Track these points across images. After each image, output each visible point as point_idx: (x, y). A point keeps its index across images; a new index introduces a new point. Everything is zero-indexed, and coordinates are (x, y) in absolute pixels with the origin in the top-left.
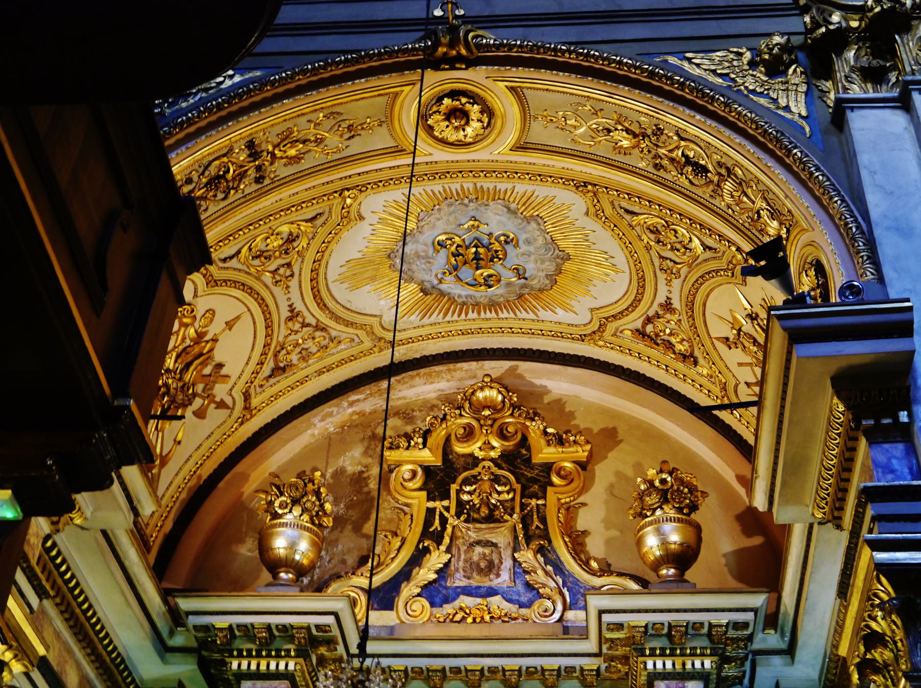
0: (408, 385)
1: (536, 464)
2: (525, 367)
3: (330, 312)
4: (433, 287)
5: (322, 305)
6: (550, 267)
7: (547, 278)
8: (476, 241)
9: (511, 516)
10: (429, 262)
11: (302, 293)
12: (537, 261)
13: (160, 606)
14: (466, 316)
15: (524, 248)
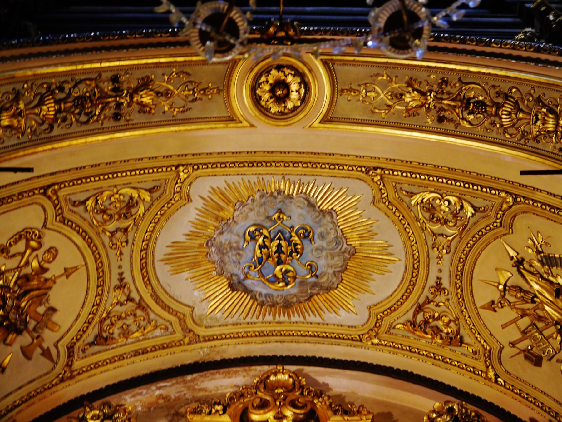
0: (210, 378)
2: (308, 370)
3: (152, 289)
4: (240, 282)
5: (148, 282)
6: (338, 263)
7: (335, 275)
8: (280, 234)
10: (239, 254)
11: (131, 264)
12: (328, 256)
14: (263, 319)
15: (318, 242)
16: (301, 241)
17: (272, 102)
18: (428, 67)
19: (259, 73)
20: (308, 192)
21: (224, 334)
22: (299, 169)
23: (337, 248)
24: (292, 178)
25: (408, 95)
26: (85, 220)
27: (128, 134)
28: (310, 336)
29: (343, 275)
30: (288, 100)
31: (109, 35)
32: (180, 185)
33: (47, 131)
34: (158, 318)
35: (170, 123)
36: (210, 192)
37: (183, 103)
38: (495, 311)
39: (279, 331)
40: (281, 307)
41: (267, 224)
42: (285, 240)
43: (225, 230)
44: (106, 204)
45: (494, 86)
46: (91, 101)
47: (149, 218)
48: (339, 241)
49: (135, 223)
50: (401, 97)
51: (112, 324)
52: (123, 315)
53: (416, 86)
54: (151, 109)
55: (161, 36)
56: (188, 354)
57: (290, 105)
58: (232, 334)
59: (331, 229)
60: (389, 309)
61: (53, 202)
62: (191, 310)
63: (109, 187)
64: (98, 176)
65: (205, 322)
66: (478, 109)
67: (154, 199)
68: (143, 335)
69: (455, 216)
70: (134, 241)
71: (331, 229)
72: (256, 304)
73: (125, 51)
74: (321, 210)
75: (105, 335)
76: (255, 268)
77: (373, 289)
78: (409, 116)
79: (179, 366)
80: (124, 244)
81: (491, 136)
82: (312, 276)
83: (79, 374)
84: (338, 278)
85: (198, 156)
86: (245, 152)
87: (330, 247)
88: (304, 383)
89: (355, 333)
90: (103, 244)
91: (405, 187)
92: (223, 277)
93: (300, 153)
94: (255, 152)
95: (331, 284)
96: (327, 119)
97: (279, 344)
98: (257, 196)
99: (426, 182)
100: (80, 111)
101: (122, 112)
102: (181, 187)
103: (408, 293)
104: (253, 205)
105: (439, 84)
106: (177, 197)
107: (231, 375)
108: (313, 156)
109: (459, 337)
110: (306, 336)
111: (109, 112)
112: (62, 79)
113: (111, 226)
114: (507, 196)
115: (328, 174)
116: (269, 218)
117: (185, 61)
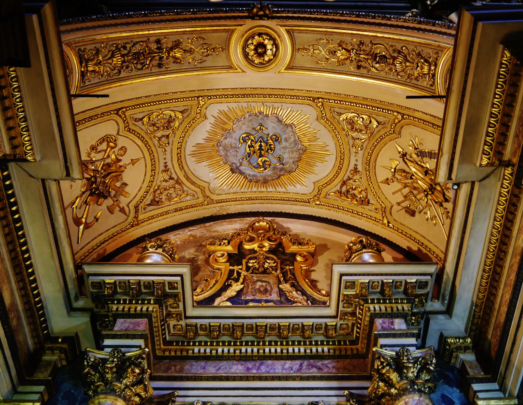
1: (287, 253)
2: (278, 219)
4: (237, 168)
5: (182, 168)
9: (276, 272)
10: (236, 151)
12: (289, 152)
13: (72, 272)
15: (284, 144)
16: (274, 143)
18: (352, 34)
24: (268, 104)
25: (339, 52)
28: (279, 200)
37: (201, 57)
39: (261, 197)
41: (253, 132)
42: (264, 142)
44: (155, 120)
45: (392, 46)
46: (144, 55)
51: (161, 193)
52: (168, 188)
53: (344, 46)
55: (186, 14)
56: (207, 210)
57: (267, 59)
61: (123, 119)
62: (208, 184)
64: (150, 103)
65: (216, 192)
66: (382, 60)
67: (184, 117)
69: (366, 127)
72: (247, 181)
74: (286, 124)
75: (157, 199)
77: (316, 172)
80: (167, 145)
83: (142, 222)
84: (295, 165)
87: (291, 147)
89: (305, 198)
90: (154, 144)
91: (337, 110)
96: (289, 67)
98: (247, 116)
105: (358, 44)
110: (277, 200)
111: (155, 63)
112: (125, 41)
113: (159, 134)
117: (202, 30)
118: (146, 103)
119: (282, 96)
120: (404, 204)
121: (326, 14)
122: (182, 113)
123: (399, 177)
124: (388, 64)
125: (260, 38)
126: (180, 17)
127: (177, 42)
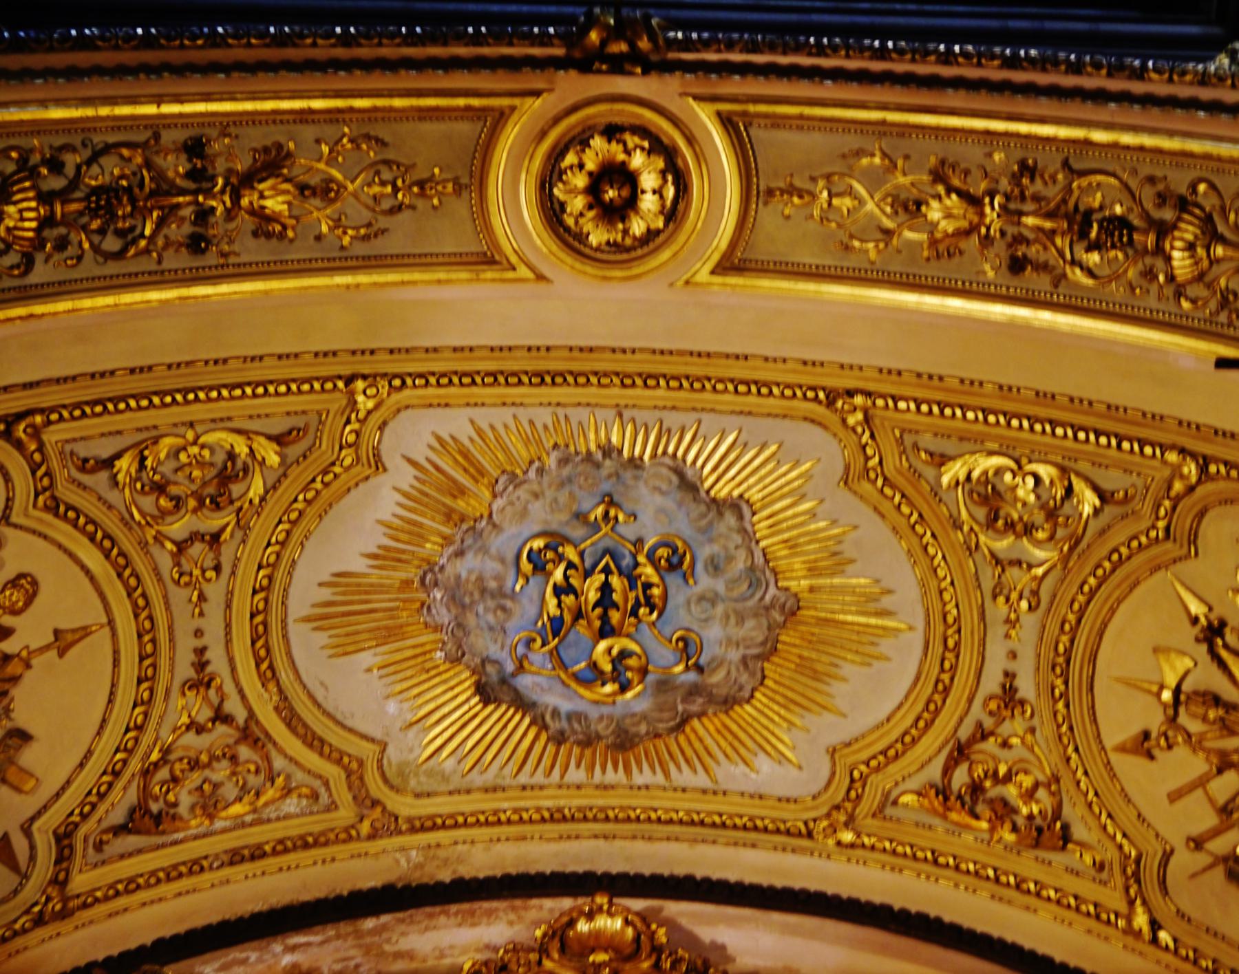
0: (423, 926)
2: (675, 909)
3: (281, 691)
4: (503, 681)
5: (269, 676)
6: (754, 634)
8: (607, 558)
10: (503, 609)
11: (228, 626)
12: (727, 617)
14: (562, 777)
15: (704, 582)
16: (662, 578)
17: (593, 219)
18: (988, 133)
19: (562, 145)
20: (680, 453)
21: (463, 814)
22: (661, 392)
23: (752, 595)
24: (641, 416)
25: (934, 204)
26: (110, 507)
27: (224, 288)
28: (681, 822)
29: (766, 665)
30: (632, 215)
31: (181, 36)
32: (356, 426)
33: (16, 272)
34: (292, 768)
35: (332, 264)
36: (431, 447)
37: (366, 215)
38: (1151, 757)
39: (602, 809)
40: (608, 747)
41: (577, 532)
42: (621, 573)
43: (469, 547)
44: (167, 469)
45: (1151, 180)
46: (133, 201)
47: (276, 508)
48: (759, 580)
49: (238, 521)
50: (919, 209)
51: (175, 780)
52: (204, 758)
53: (956, 182)
54: (285, 227)
55: (314, 45)
56: (369, 863)
57: (638, 227)
58: (483, 813)
59: (737, 547)
60: (884, 752)
61: (29, 458)
62: (377, 749)
63: (175, 425)
64: (147, 396)
65: (413, 783)
66: (1112, 235)
67: (289, 461)
68: (255, 811)
69: (1051, 514)
70: (235, 566)
71: (737, 547)
72: (544, 737)
73: (222, 76)
74: (714, 500)
75: (155, 807)
76: (543, 645)
77: (840, 703)
78: (938, 257)
79: (345, 893)
80: (211, 574)
81: (1142, 304)
82: (687, 668)
83: (85, 906)
84: (753, 674)
85: (403, 356)
86: (522, 347)
87: (735, 594)
88: (664, 940)
89: (794, 817)
90: (156, 571)
91: (927, 440)
92: (461, 667)
93: (662, 352)
94: (548, 349)
95: (736, 687)
96: (729, 265)
97: (601, 842)
98: (551, 461)
99: (980, 427)
100: (103, 223)
101: (211, 232)
102: (358, 433)
103: (932, 711)
104: (540, 483)
105: (1014, 175)
106: (348, 457)
107: (476, 920)
108: (695, 359)
109: (1058, 825)
110: (671, 821)
111: (175, 231)
112: (59, 141)
113: (178, 528)
114: (1184, 459)
115: (731, 408)
116: (580, 517)
117: (375, 109)
118: (133, 396)
119: (696, 382)
120: (1219, 846)
121: (882, 54)
122: (279, 443)
123: (1195, 727)
124: (1136, 251)
125: (614, 144)
126: (291, 53)
127: (274, 153)
